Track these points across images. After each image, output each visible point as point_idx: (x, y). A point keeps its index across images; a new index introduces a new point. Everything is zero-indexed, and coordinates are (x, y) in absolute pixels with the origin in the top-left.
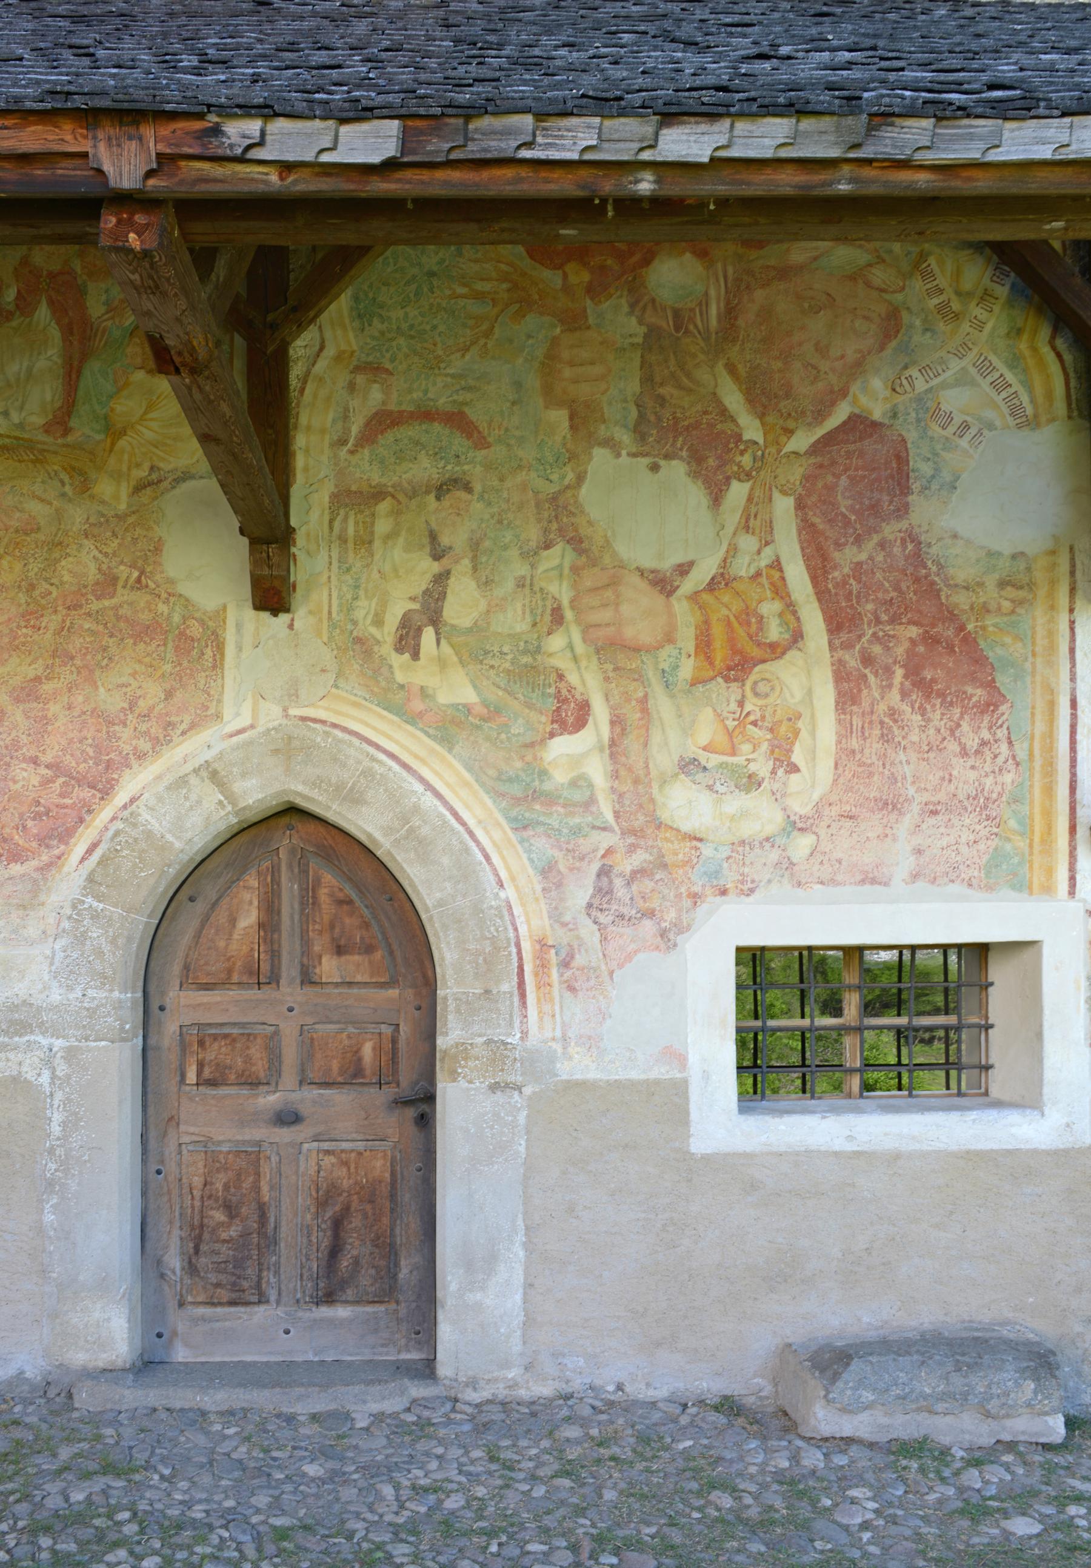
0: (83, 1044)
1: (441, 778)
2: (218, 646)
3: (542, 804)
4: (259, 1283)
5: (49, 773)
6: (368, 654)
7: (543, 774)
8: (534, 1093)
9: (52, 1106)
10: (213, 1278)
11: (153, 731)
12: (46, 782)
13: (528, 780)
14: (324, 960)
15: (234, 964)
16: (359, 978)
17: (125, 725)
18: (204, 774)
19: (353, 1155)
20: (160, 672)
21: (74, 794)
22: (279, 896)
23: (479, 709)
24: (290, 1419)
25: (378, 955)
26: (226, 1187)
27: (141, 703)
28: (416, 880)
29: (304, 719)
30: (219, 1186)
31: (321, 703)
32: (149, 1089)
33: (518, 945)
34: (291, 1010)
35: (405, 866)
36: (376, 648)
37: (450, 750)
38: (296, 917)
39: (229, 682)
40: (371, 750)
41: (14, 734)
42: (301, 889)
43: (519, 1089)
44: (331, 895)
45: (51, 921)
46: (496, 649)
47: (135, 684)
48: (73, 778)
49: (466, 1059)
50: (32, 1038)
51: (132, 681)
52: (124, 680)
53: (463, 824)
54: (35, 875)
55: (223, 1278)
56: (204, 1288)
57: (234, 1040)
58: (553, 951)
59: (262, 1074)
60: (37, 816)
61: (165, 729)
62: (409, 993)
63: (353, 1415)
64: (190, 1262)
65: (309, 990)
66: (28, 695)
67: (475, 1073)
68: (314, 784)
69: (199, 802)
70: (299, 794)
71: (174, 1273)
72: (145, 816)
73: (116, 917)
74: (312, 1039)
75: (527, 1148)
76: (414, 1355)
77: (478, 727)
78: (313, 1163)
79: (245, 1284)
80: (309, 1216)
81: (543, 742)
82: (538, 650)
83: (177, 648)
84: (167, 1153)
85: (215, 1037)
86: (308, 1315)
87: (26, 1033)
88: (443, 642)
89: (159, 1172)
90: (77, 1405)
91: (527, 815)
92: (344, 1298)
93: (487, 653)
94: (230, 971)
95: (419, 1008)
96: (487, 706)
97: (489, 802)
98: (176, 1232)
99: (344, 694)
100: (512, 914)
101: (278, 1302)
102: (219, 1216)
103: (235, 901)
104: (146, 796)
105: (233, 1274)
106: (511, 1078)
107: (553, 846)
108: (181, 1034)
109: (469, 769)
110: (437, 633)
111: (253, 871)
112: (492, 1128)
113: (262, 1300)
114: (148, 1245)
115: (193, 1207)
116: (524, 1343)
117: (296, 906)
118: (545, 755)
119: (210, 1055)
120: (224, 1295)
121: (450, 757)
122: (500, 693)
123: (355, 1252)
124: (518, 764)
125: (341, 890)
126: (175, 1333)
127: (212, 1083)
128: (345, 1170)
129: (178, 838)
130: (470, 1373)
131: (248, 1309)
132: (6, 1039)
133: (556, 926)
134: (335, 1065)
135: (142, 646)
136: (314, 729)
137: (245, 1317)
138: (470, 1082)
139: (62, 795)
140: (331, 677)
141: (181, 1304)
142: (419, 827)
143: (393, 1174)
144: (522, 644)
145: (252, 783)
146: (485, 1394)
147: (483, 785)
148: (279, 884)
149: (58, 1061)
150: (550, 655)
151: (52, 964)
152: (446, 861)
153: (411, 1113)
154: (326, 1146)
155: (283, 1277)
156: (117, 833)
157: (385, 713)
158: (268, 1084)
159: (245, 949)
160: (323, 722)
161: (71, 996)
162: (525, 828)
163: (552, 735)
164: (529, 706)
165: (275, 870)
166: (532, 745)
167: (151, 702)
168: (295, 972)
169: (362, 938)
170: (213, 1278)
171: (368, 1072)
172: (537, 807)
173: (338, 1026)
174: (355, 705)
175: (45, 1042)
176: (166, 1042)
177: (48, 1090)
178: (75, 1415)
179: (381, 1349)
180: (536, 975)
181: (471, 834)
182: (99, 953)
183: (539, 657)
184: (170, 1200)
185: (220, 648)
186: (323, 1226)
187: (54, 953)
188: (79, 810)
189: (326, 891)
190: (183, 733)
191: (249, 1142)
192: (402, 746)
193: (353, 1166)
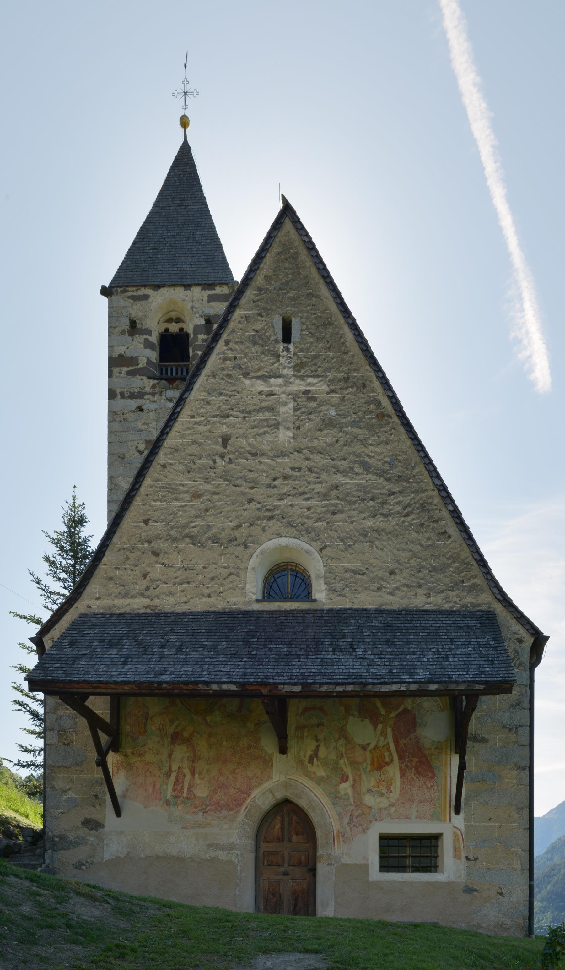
7: (339, 792)
12: (237, 792)
43: (333, 865)
60: (235, 800)
72: (257, 801)
85: (271, 854)
102: (271, 896)
127: (270, 865)
149: (239, 857)
154: (294, 881)
163: (341, 783)
166: (336, 785)
185: (272, 762)
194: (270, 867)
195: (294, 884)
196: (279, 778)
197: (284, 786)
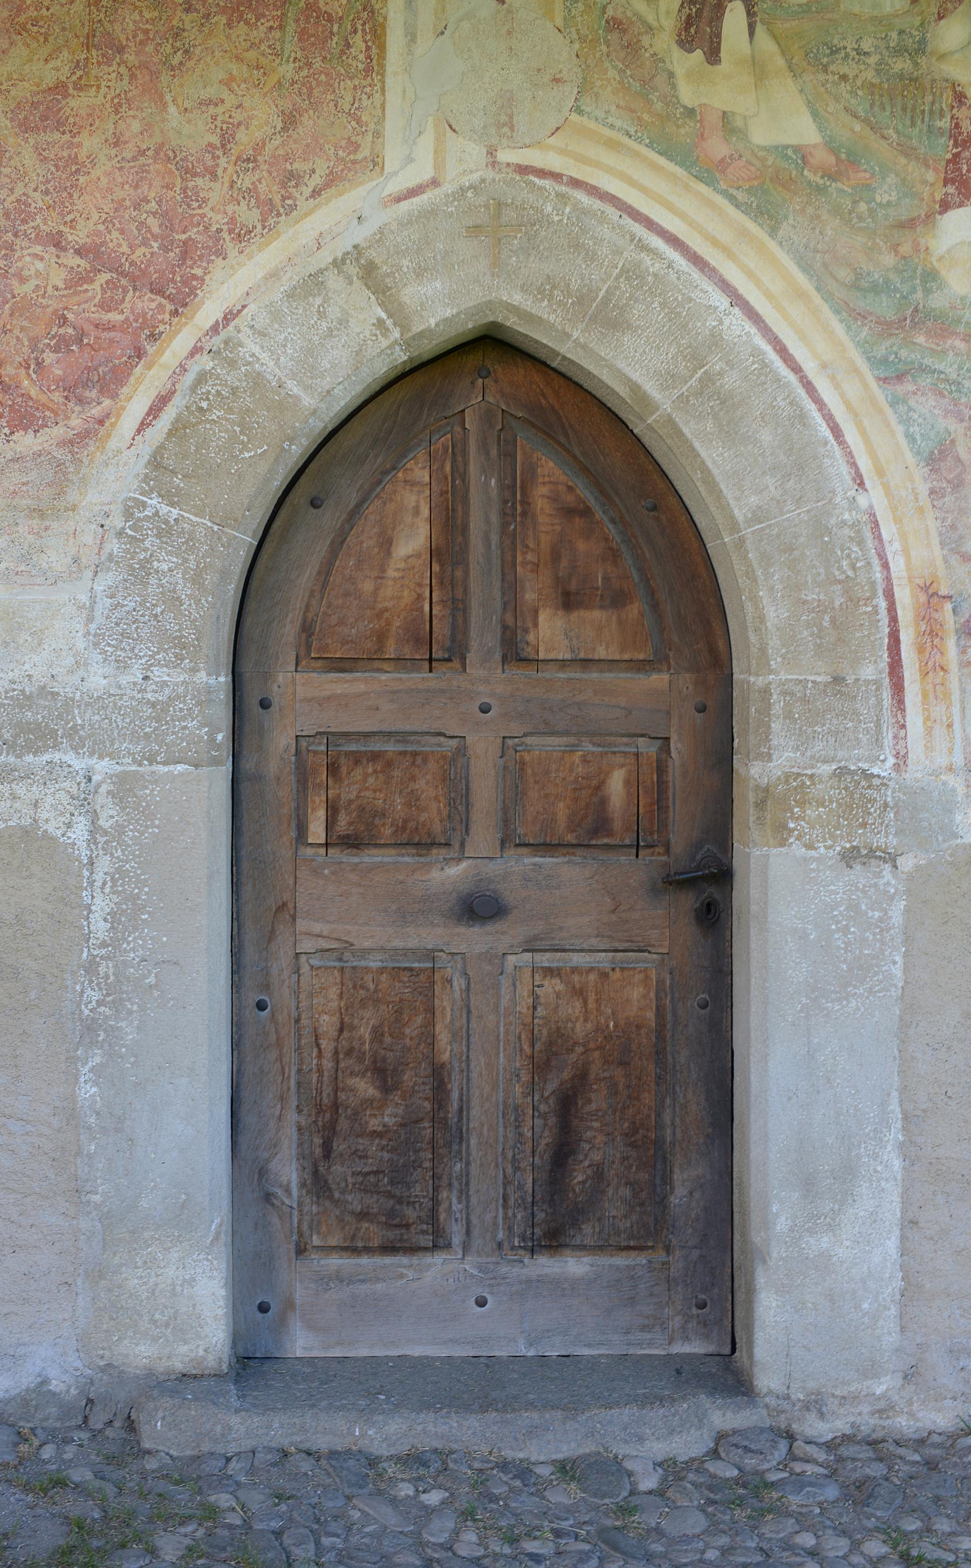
0: (146, 769)
1: (758, 283)
2: (374, 31)
3: (928, 334)
4: (434, 1212)
5: (82, 263)
6: (632, 49)
7: (931, 278)
8: (918, 868)
9: (92, 883)
10: (355, 1202)
11: (262, 188)
12: (77, 280)
13: (905, 289)
14: (543, 617)
15: (388, 624)
16: (601, 653)
17: (214, 176)
18: (352, 270)
19: (592, 977)
20: (273, 80)
21: (127, 305)
22: (465, 500)
23: (822, 157)
24: (524, 1471)
25: (634, 609)
26: (377, 1034)
27: (241, 135)
28: (715, 471)
29: (523, 170)
30: (365, 1032)
31: (552, 141)
32: (243, 853)
33: (889, 595)
34: (485, 709)
35: (697, 445)
36: (646, 40)
37: (773, 232)
38: (495, 538)
39: (393, 99)
40: (639, 230)
41: (19, 189)
42: (501, 486)
43: (892, 859)
44: (554, 498)
45: (88, 539)
46: (850, 45)
47: (231, 100)
48: (123, 274)
49: (802, 804)
50: (57, 756)
51: (225, 94)
52: (211, 92)
53: (796, 369)
54: (59, 454)
55: (372, 1202)
56: (340, 1220)
57: (389, 764)
58: (948, 607)
59: (437, 828)
60: (62, 344)
61: (284, 185)
62: (686, 681)
63: (629, 1465)
64: (316, 1173)
65: (518, 673)
66: (44, 118)
67: (818, 831)
68: (541, 291)
69: (343, 322)
70: (516, 310)
71: (288, 1191)
72: (251, 346)
73: (200, 533)
74: (523, 763)
75: (906, 970)
76: (695, 1347)
77: (820, 190)
78: (524, 991)
79: (411, 1214)
80: (518, 1089)
81: (929, 219)
82: (921, 48)
83: (302, 35)
84: (274, 972)
85: (357, 759)
86: (515, 1271)
87: (45, 749)
88: (760, 29)
89: (261, 1006)
90: (147, 1445)
91: (904, 353)
92: (577, 1241)
93: (834, 51)
94: (381, 637)
95: (702, 709)
96: (834, 152)
97: (839, 329)
98: (292, 1117)
99: (593, 125)
100: (879, 537)
101: (466, 1248)
102: (365, 1087)
103: (390, 507)
104: (252, 308)
105: (390, 1195)
106: (879, 841)
107: (947, 413)
108: (298, 753)
109: (806, 268)
110: (750, 14)
111: (422, 454)
112: (845, 930)
113: (439, 1243)
114: (243, 1140)
115: (320, 1071)
116: (903, 1329)
117: (495, 518)
118: (932, 244)
119: (348, 791)
120: (375, 1233)
121: (772, 245)
122: (857, 127)
123: (596, 1156)
124: (889, 260)
125: (570, 489)
126: (290, 1305)
127: (352, 842)
128: (578, 1004)
129: (307, 388)
130: (811, 1384)
131: (415, 1260)
132: (12, 759)
133: (954, 560)
134: (562, 811)
135: (242, 29)
136: (541, 188)
137: (410, 1274)
138: (810, 846)
139: (105, 306)
140: (569, 92)
141: (301, 1251)
142: (721, 374)
143: (660, 1012)
144: (894, 35)
145: (433, 287)
146: (839, 1425)
147: (828, 297)
148: (464, 477)
149: (102, 799)
150: (942, 57)
151: (90, 619)
152: (766, 437)
153: (688, 901)
154: (545, 959)
155: (474, 1200)
156: (202, 378)
157: (662, 161)
158: (447, 845)
159: (407, 596)
160: (556, 176)
161: (124, 680)
162: (900, 377)
163: (945, 206)
164: (906, 151)
165: (458, 451)
166: (909, 224)
167: (258, 135)
168: (492, 640)
169: (606, 579)
170: (355, 1202)
171: (617, 825)
172: (921, 339)
173: (564, 740)
174: (612, 145)
175: (79, 764)
176: (272, 767)
177: (84, 854)
178: (151, 1464)
179: (641, 1336)
180: (921, 650)
181: (809, 387)
182: (172, 600)
183: (923, 61)
184: (280, 1058)
185: (378, 35)
186: (543, 1108)
187: (93, 599)
188: (136, 334)
189: (544, 490)
190: (316, 193)
191: (413, 951)
192: (691, 223)
193: (592, 998)
194: (349, 858)
195: (551, 987)
196: (439, 162)
197: (475, 230)
